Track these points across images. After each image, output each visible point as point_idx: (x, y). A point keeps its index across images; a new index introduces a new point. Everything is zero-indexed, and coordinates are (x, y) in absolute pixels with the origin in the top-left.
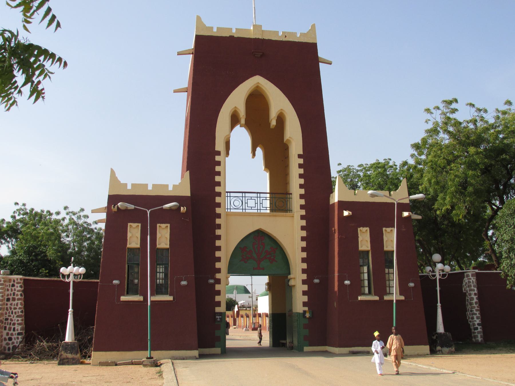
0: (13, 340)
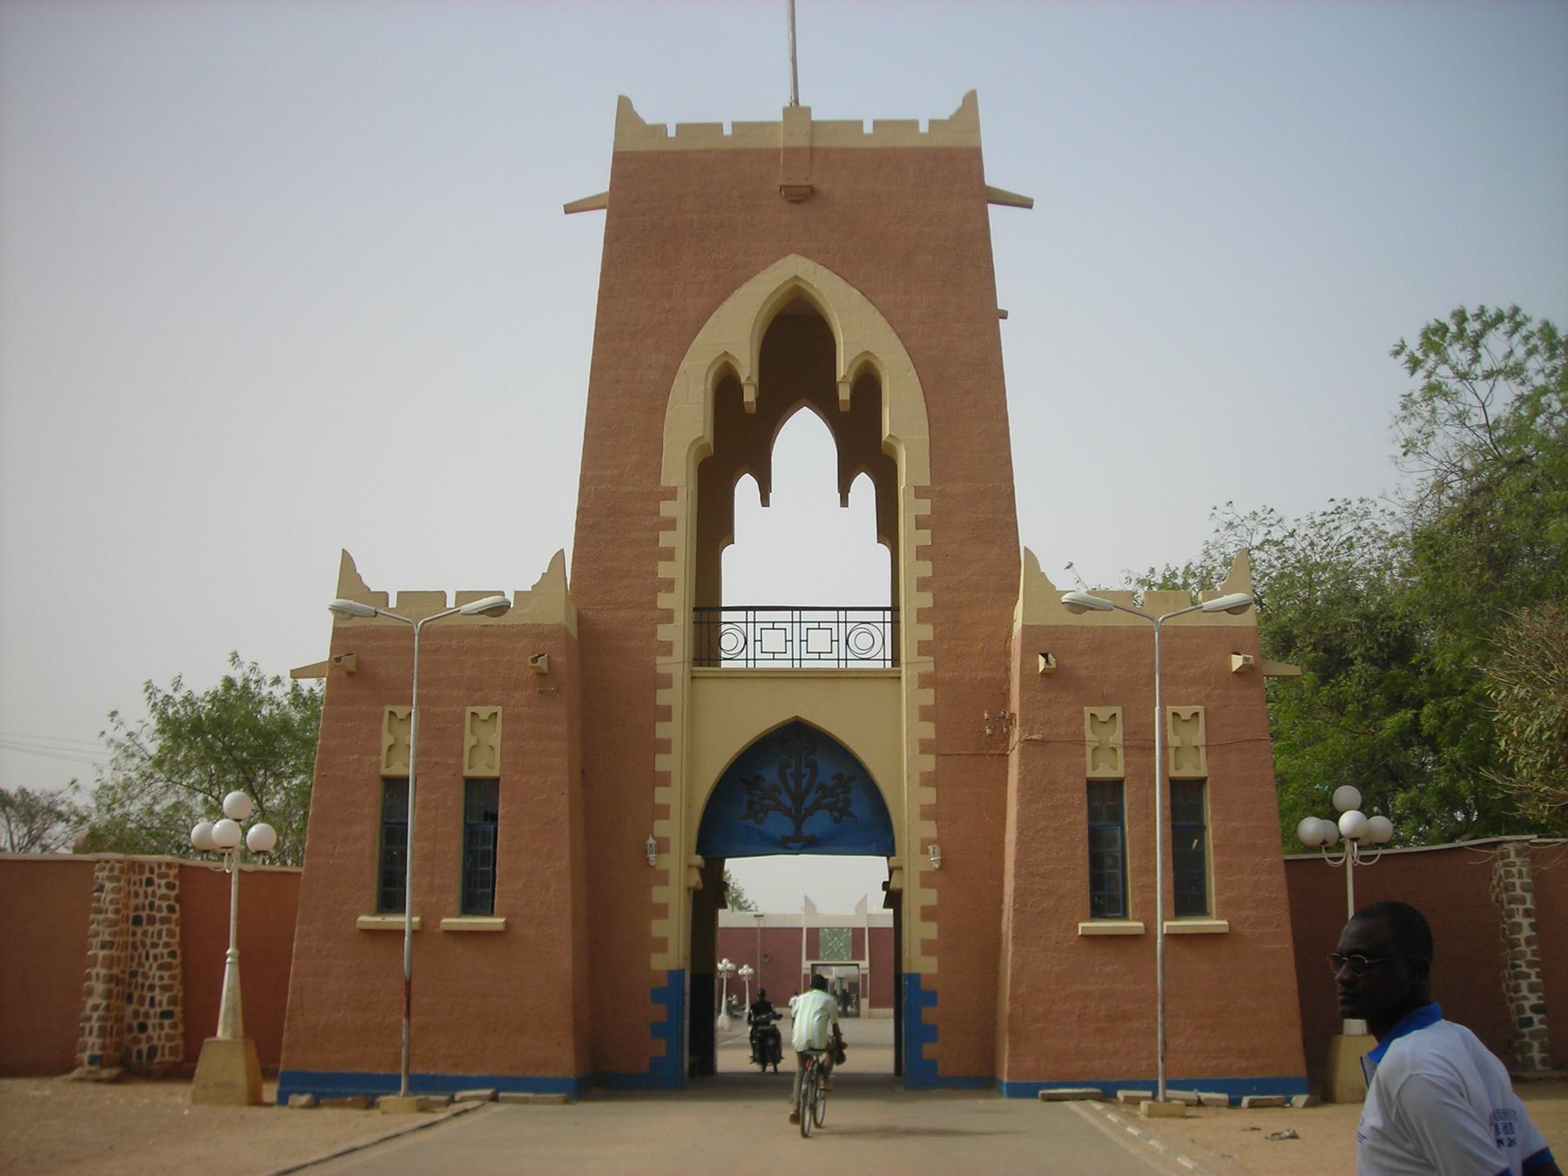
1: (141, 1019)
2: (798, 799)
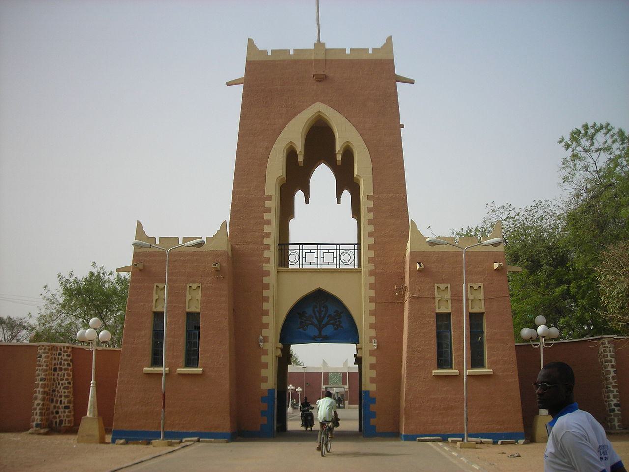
0: (60, 414)
1: (57, 409)
2: (320, 321)
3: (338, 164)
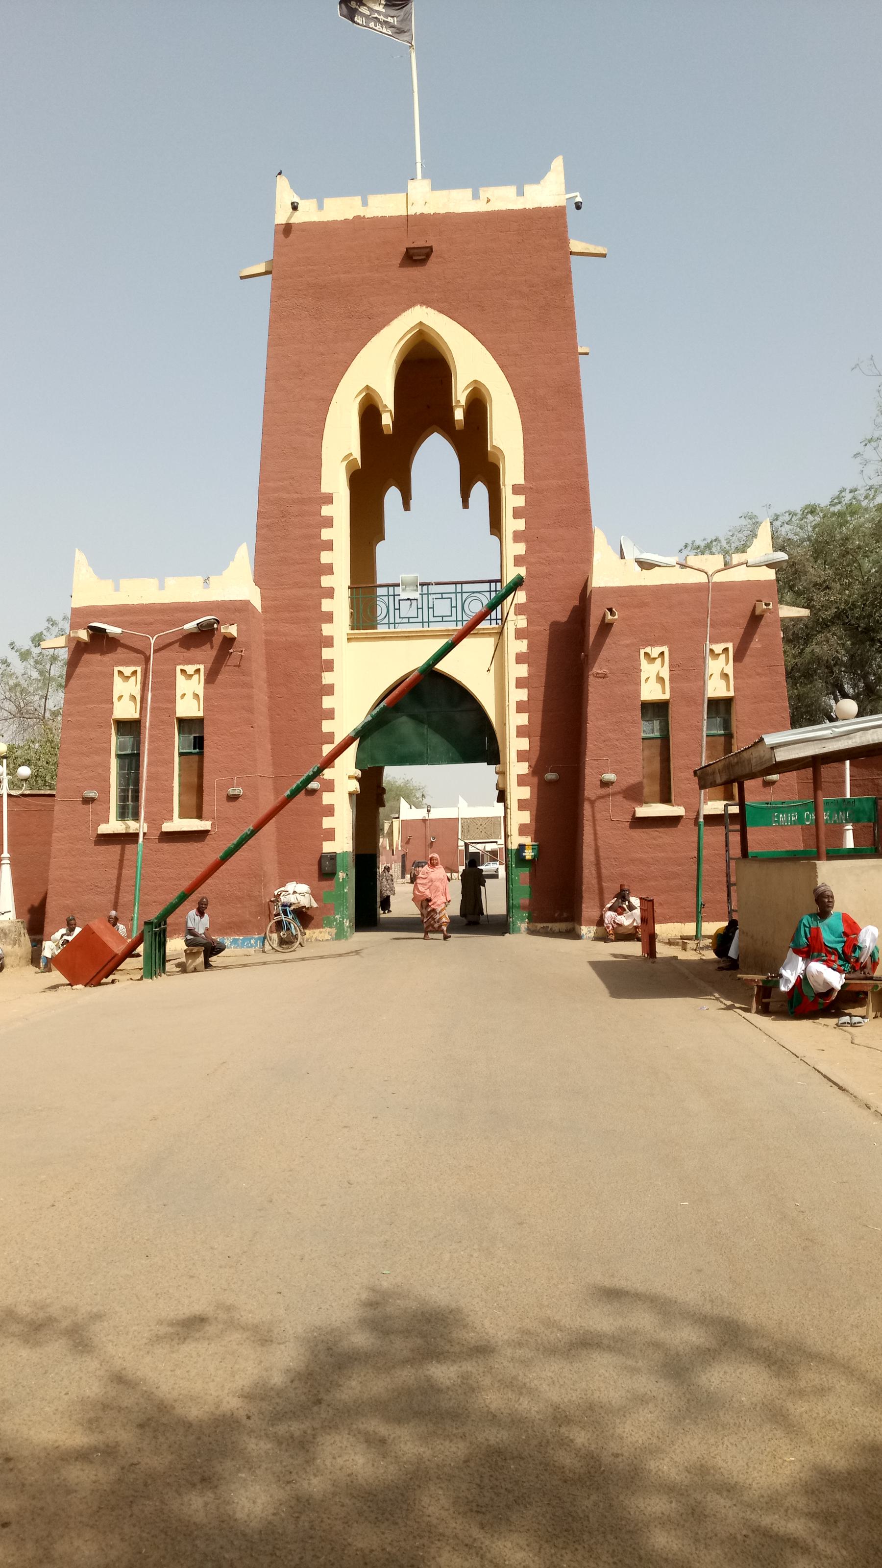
3: (457, 428)
